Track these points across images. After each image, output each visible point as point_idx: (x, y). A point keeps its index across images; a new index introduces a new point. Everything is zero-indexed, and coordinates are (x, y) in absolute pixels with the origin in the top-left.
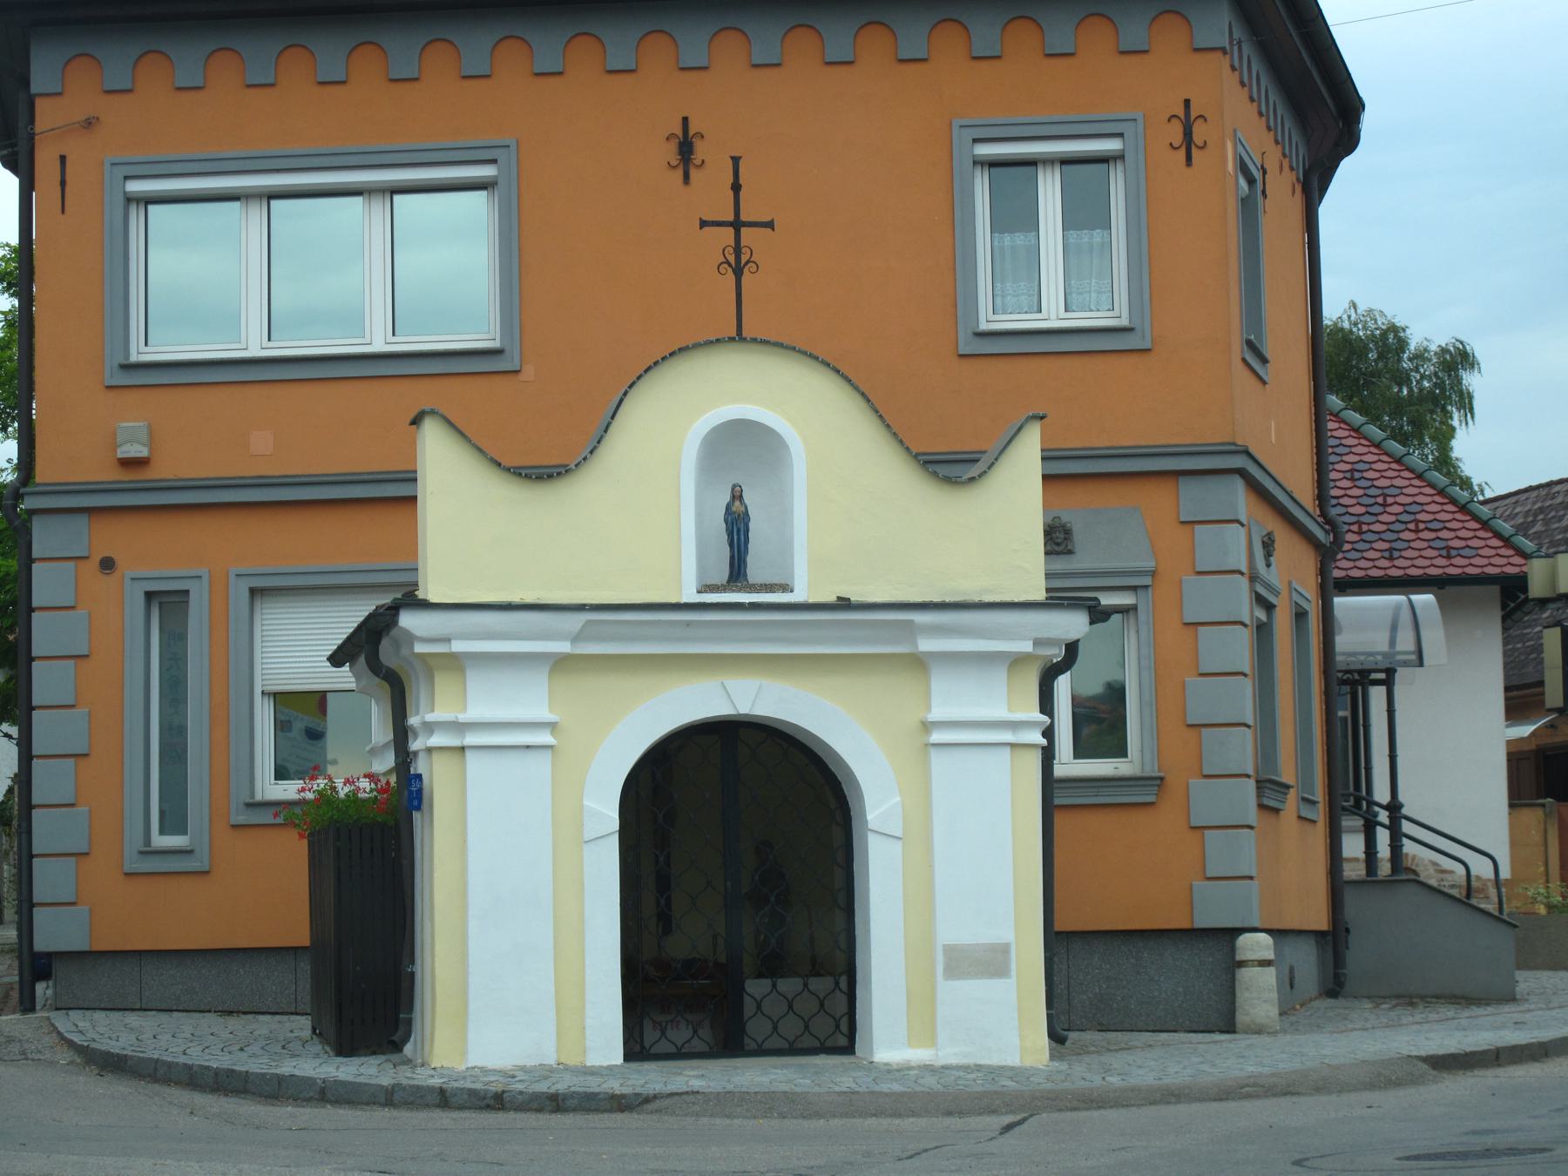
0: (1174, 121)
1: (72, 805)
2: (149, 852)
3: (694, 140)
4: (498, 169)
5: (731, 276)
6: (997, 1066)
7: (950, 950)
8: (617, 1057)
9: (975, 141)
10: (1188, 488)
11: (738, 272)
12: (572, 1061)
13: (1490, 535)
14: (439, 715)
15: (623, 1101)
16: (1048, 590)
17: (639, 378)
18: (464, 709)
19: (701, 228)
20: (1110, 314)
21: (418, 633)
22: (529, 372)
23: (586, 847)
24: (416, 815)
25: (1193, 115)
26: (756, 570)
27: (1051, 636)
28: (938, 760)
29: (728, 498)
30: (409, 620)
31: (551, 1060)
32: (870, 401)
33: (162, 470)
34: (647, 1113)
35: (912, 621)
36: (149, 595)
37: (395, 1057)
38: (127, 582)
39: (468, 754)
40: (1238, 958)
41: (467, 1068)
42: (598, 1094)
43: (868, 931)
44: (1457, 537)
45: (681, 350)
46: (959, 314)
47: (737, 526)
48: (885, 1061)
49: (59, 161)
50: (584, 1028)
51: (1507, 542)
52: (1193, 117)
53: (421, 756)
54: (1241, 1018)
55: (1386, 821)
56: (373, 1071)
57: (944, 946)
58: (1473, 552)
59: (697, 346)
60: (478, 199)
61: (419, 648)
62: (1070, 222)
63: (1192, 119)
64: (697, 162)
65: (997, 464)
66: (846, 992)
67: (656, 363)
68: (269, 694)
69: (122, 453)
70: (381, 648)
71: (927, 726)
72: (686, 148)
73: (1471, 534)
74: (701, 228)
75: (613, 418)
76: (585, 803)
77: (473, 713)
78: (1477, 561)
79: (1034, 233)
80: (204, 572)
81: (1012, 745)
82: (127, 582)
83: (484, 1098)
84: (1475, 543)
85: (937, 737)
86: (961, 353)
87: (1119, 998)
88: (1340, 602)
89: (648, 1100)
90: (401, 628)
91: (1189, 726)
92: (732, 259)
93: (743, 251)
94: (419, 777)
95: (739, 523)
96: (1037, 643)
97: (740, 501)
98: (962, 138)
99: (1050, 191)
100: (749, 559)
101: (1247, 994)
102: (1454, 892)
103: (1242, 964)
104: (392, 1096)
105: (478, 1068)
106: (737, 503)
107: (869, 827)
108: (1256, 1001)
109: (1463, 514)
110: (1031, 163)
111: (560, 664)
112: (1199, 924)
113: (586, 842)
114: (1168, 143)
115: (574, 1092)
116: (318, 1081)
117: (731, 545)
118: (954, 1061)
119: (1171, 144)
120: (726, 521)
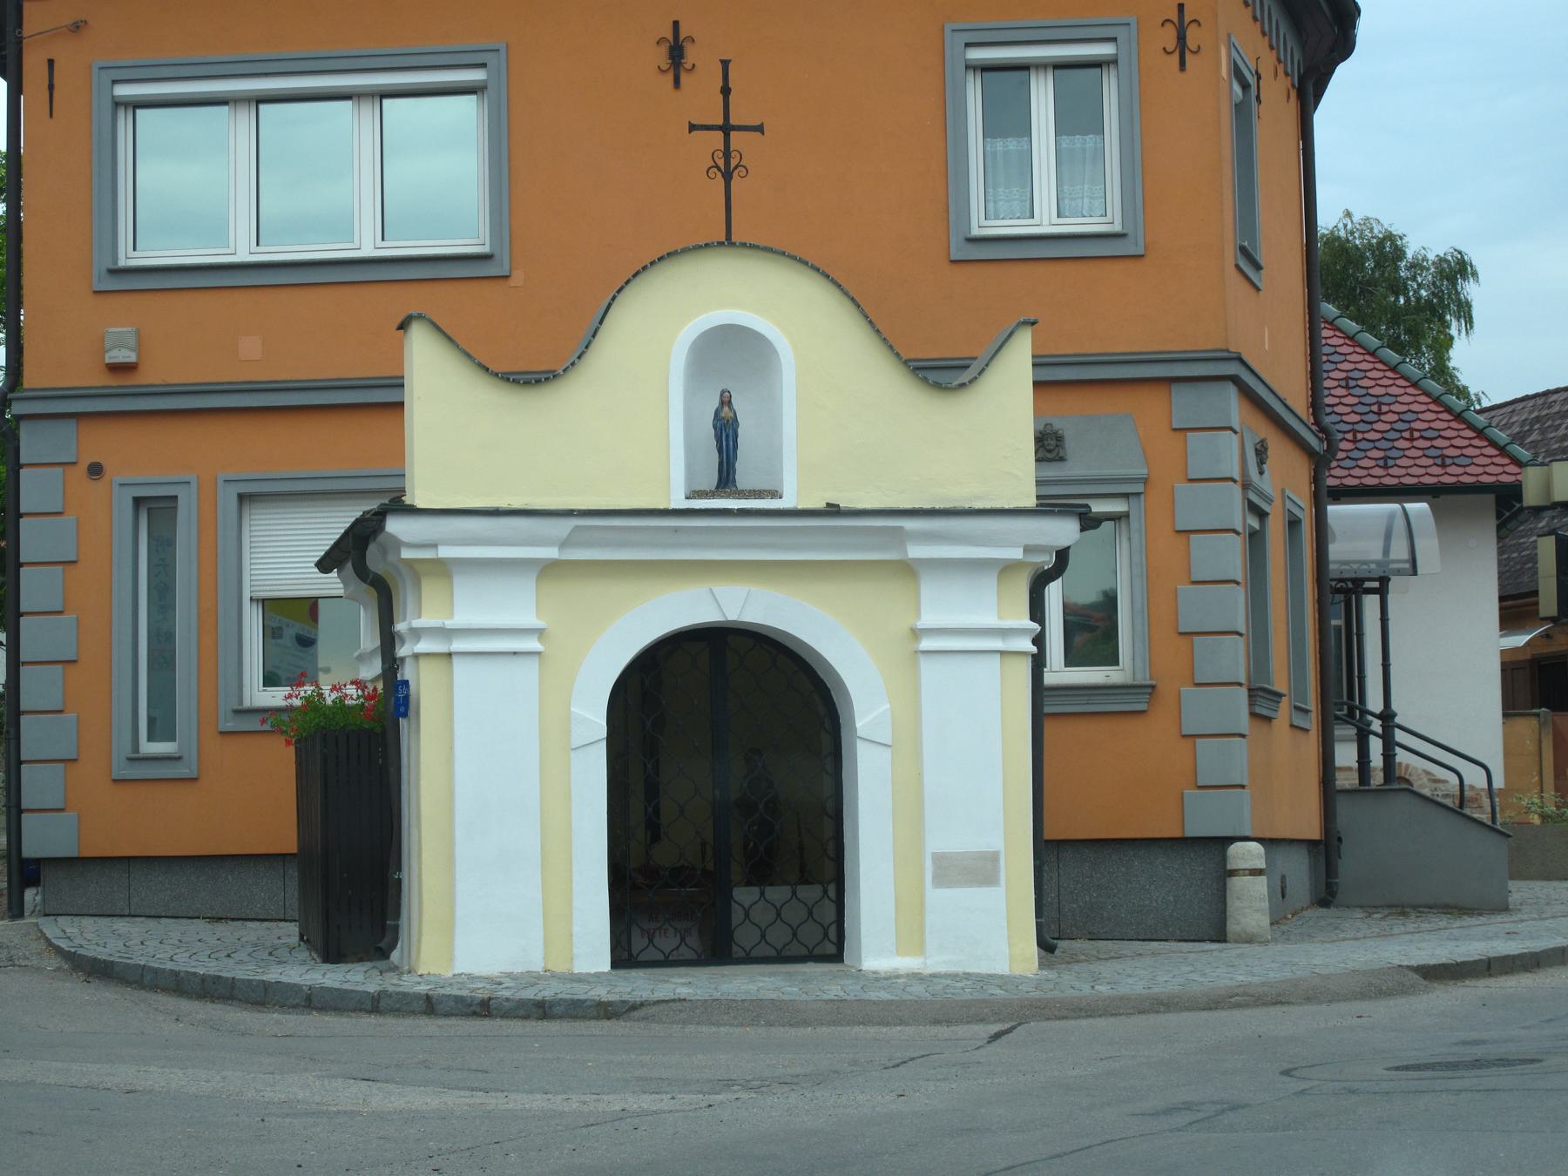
0: (1168, 25)
1: (61, 712)
2: (137, 759)
6: (987, 974)
7: (940, 860)
10: (1181, 395)
11: (728, 176)
12: (560, 967)
14: (425, 621)
16: (1038, 497)
17: (628, 282)
18: (452, 615)
19: (690, 132)
22: (518, 278)
23: (573, 754)
26: (743, 479)
28: (928, 668)
29: (716, 403)
30: (395, 526)
31: (537, 966)
33: (150, 376)
35: (901, 528)
36: (138, 502)
38: (116, 488)
39: (457, 663)
42: (585, 1001)
44: (1452, 446)
47: (726, 432)
50: (571, 935)
51: (1502, 450)
54: (1232, 928)
57: (933, 854)
59: (686, 251)
60: (466, 106)
61: (406, 554)
62: (1064, 125)
63: (1186, 24)
64: (688, 66)
67: (645, 268)
69: (110, 358)
70: (368, 553)
71: (917, 634)
74: (690, 132)
76: (572, 709)
77: (460, 619)
79: (1026, 139)
80: (192, 478)
81: (1002, 653)
82: (116, 488)
83: (471, 1005)
84: (1470, 452)
85: (927, 644)
86: (952, 259)
87: (1110, 907)
88: (1332, 509)
89: (635, 1007)
90: (388, 533)
91: (1181, 634)
92: (721, 163)
93: (733, 155)
94: (406, 683)
96: (1028, 549)
99: (1042, 96)
100: (737, 465)
101: (1238, 904)
103: (1233, 873)
106: (726, 409)
107: (859, 733)
110: (1023, 67)
111: (548, 570)
112: (1188, 834)
114: (1163, 46)
115: (560, 999)
117: (720, 450)
118: (942, 969)
119: (1164, 49)
120: (715, 427)
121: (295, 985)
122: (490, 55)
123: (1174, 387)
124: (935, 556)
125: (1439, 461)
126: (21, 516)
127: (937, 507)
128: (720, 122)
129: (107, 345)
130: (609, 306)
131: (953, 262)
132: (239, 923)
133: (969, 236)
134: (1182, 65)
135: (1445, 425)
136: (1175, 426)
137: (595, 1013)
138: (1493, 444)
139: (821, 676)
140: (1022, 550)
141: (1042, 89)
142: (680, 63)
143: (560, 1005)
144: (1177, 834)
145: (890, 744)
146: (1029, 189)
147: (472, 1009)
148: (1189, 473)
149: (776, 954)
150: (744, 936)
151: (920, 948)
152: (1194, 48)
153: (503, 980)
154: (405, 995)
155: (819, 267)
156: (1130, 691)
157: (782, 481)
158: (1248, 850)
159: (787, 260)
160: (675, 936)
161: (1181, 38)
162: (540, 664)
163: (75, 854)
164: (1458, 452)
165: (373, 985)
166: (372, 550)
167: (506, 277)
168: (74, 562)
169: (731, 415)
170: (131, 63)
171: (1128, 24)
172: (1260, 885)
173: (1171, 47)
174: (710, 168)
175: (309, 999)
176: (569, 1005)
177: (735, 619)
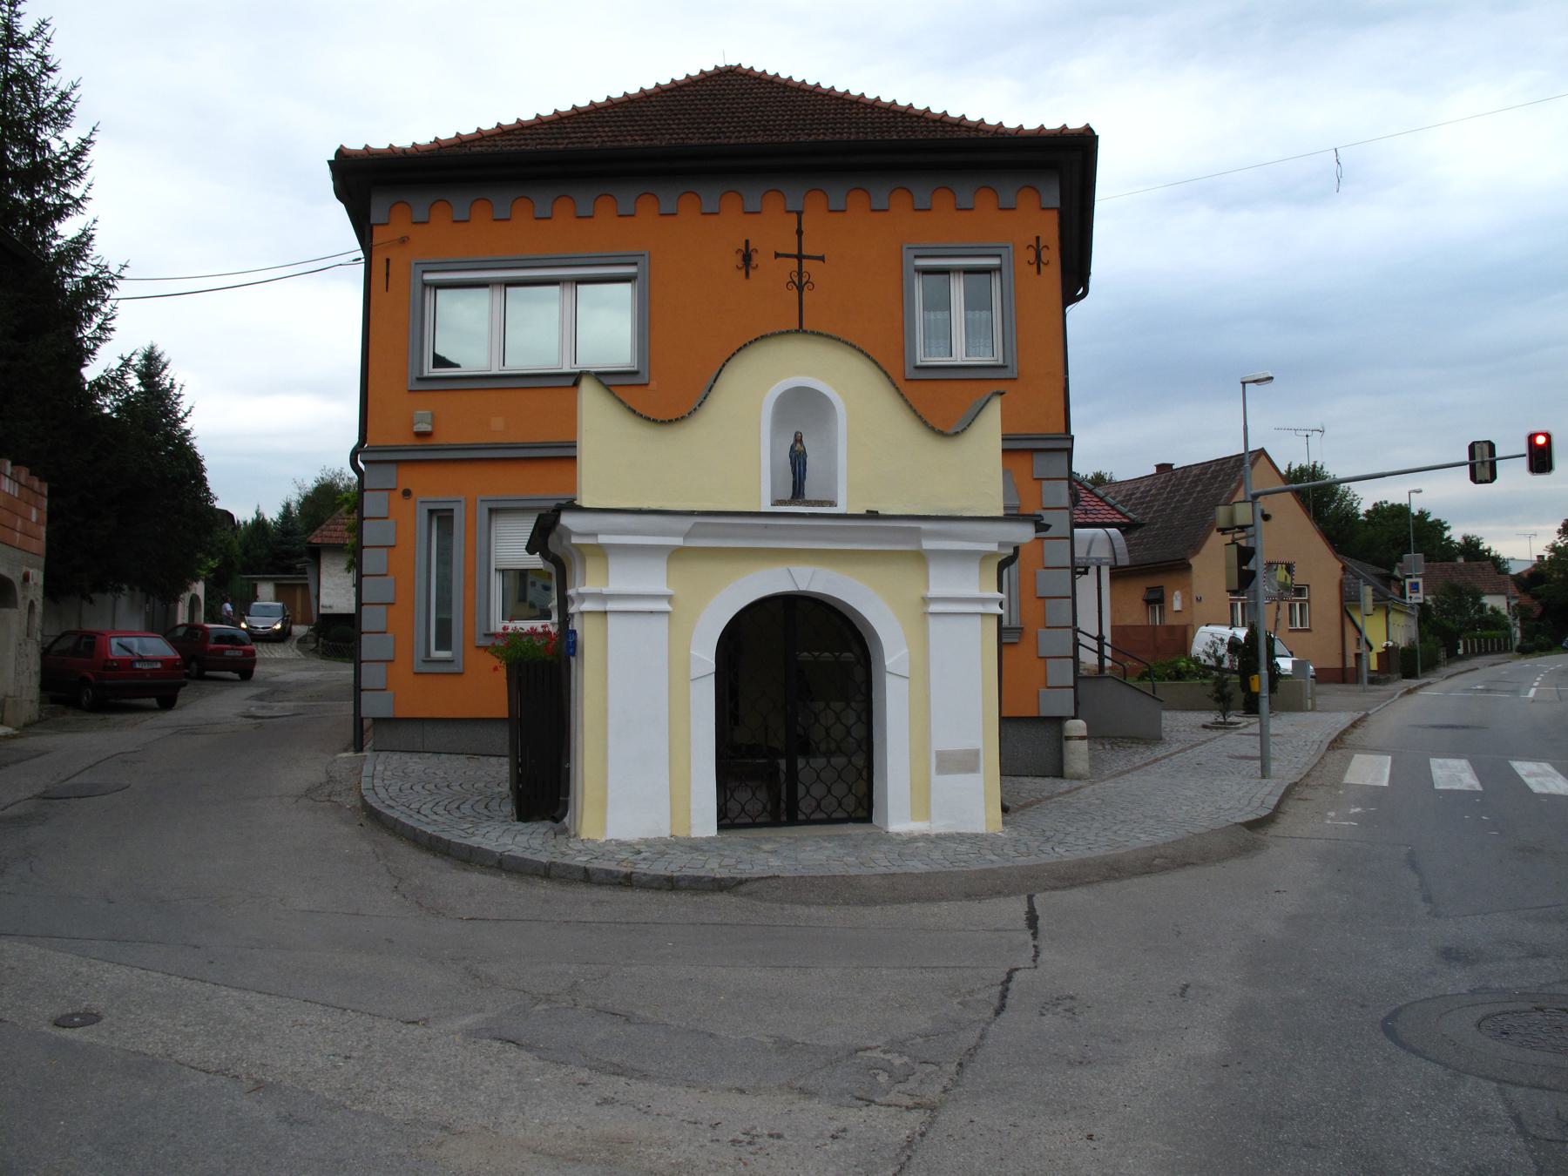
0: (1030, 248)
2: (428, 660)
5: (795, 291)
6: (972, 834)
7: (940, 754)
8: (710, 829)
9: (916, 257)
10: (1039, 460)
11: (800, 289)
12: (681, 833)
14: (589, 588)
16: (1005, 508)
17: (734, 355)
18: (607, 585)
19: (776, 258)
20: (993, 359)
21: (574, 529)
22: (653, 385)
24: (573, 659)
25: (1041, 245)
26: (810, 492)
28: (933, 623)
29: (791, 441)
30: (567, 520)
31: (666, 834)
33: (440, 439)
34: (741, 896)
35: (919, 528)
36: (431, 512)
37: (557, 826)
38: (418, 505)
39: (610, 618)
41: (606, 841)
42: (704, 877)
43: (884, 740)
45: (762, 337)
47: (798, 461)
50: (690, 811)
51: (1113, 508)
53: (576, 617)
54: (1068, 770)
55: (1106, 647)
56: (536, 843)
57: (937, 752)
58: (1097, 512)
59: (773, 335)
60: (625, 290)
61: (575, 540)
62: (969, 306)
64: (754, 265)
67: (745, 345)
68: (499, 570)
70: (550, 539)
71: (926, 601)
72: (747, 258)
74: (776, 258)
75: (715, 381)
76: (691, 652)
77: (614, 587)
78: (1099, 516)
80: (462, 498)
81: (982, 614)
82: (418, 505)
84: (1097, 508)
85: (933, 608)
88: (1077, 531)
89: (741, 882)
90: (562, 525)
92: (796, 280)
93: (804, 275)
94: (574, 632)
96: (1001, 545)
98: (908, 255)
99: (957, 287)
103: (1068, 738)
106: (798, 445)
107: (888, 669)
110: (945, 271)
111: (675, 554)
112: (1043, 714)
113: (692, 680)
117: (794, 474)
118: (942, 830)
119: (1029, 262)
121: (492, 852)
122: (639, 258)
127: (939, 514)
128: (796, 253)
130: (721, 370)
131: (907, 380)
132: (483, 759)
137: (711, 887)
138: (1108, 505)
144: (1036, 715)
145: (907, 676)
147: (619, 880)
148: (1044, 503)
150: (805, 805)
151: (927, 815)
153: (643, 848)
154: (568, 866)
157: (837, 494)
159: (842, 345)
161: (1038, 256)
162: (669, 619)
163: (392, 716)
164: (1092, 508)
165: (548, 854)
166: (552, 539)
167: (646, 385)
168: (394, 546)
169: (802, 449)
170: (427, 261)
175: (500, 862)
177: (805, 589)
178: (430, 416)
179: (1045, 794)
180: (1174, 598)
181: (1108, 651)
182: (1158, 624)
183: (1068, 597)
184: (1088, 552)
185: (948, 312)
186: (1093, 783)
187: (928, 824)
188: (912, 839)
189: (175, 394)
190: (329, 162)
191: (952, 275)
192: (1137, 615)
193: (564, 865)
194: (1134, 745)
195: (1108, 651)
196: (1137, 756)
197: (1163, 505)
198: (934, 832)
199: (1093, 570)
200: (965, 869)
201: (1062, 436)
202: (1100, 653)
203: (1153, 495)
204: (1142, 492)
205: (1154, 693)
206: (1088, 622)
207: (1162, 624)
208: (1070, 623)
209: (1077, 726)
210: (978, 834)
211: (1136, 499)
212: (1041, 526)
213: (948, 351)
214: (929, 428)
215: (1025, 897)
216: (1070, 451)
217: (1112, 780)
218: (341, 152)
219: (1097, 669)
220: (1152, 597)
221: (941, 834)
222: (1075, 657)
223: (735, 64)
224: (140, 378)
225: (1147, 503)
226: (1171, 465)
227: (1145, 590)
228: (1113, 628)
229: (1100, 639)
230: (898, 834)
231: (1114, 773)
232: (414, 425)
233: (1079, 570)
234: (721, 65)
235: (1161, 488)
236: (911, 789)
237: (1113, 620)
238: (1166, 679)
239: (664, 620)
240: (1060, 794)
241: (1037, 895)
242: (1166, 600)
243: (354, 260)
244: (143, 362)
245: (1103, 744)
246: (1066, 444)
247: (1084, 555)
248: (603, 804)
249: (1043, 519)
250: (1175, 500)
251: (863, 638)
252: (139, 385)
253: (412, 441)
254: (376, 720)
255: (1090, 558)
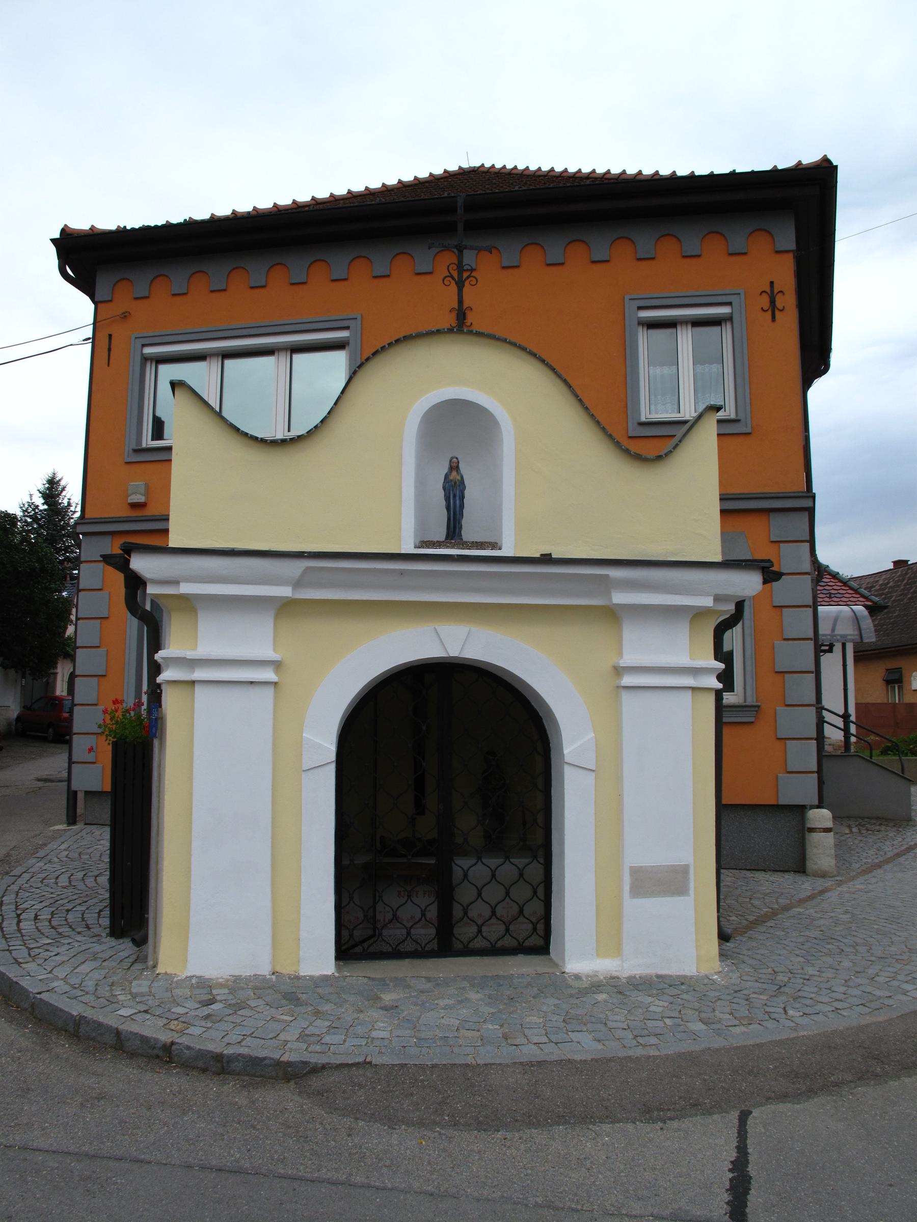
0: (764, 294)
1: (96, 705)
3: (466, 311)
4: (350, 332)
5: (454, 288)
7: (636, 872)
9: (640, 308)
10: (777, 521)
12: (287, 969)
13: (848, 588)
15: (289, 1069)
18: (195, 648)
23: (304, 775)
26: (469, 532)
27: (730, 593)
28: (629, 701)
29: (445, 470)
31: (265, 970)
32: (571, 387)
35: (607, 576)
40: (808, 825)
42: (265, 1059)
44: (833, 589)
46: (629, 414)
48: (576, 972)
49: (108, 338)
52: (776, 292)
54: (810, 865)
57: (631, 868)
58: (841, 596)
62: (697, 360)
63: (775, 294)
65: (681, 445)
66: (543, 936)
67: (383, 348)
69: (131, 499)
71: (619, 671)
73: (839, 588)
76: (304, 735)
77: (203, 650)
79: (675, 367)
81: (693, 689)
83: (154, 1048)
84: (841, 591)
85: (627, 680)
86: (630, 435)
87: (728, 848)
89: (316, 1070)
91: (777, 672)
92: (455, 275)
95: (455, 490)
96: (717, 599)
97: (457, 471)
98: (631, 306)
100: (464, 522)
101: (815, 850)
102: (839, 753)
103: (811, 830)
104: (79, 1029)
105: (197, 977)
106: (454, 473)
107: (567, 759)
108: (822, 856)
109: (835, 580)
112: (782, 802)
114: (760, 307)
115: (239, 1055)
116: (31, 995)
119: (762, 308)
120: (444, 488)
122: (351, 321)
123: (771, 514)
124: (637, 602)
125: (828, 595)
126: (79, 591)
129: (130, 492)
133: (639, 421)
134: (773, 319)
135: (829, 580)
136: (772, 539)
139: (535, 706)
140: (712, 598)
141: (684, 337)
142: (464, 323)
143: (238, 1061)
144: (773, 802)
145: (594, 769)
146: (677, 396)
147: (156, 1051)
149: (490, 946)
152: (781, 308)
155: (536, 352)
156: (745, 709)
158: (822, 816)
160: (424, 897)
161: (773, 302)
162: (275, 690)
164: (836, 592)
168: (107, 618)
169: (459, 478)
171: (739, 294)
172: (829, 838)
173: (766, 306)
174: (446, 277)
176: (247, 1062)
178: (143, 487)
179: (783, 901)
180: (912, 678)
181: (853, 729)
182: (897, 702)
183: (812, 672)
184: (833, 630)
185: (675, 367)
186: (840, 883)
187: (619, 963)
188: (596, 985)
189: (71, 511)
190: (53, 241)
191: (679, 328)
192: (877, 694)
193: (94, 1022)
194: (883, 828)
195: (853, 729)
196: (888, 843)
197: (901, 595)
198: (625, 974)
199: (838, 648)
200: (653, 1052)
201: (804, 494)
202: (846, 730)
203: (891, 587)
204: (881, 585)
205: (903, 773)
206: (833, 699)
207: (901, 702)
208: (813, 701)
209: (821, 817)
210: (685, 977)
211: (876, 591)
212: (770, 575)
213: (676, 407)
214: (623, 450)
215: (734, 1115)
216: (811, 511)
217: (861, 879)
218: (65, 231)
219: (843, 744)
220: (891, 677)
221: (634, 977)
222: (820, 738)
223: (478, 165)
224: (44, 498)
225: (886, 595)
226: (907, 561)
227: (885, 670)
228: (857, 705)
229: (846, 717)
230: (577, 977)
231: (864, 868)
232: (128, 496)
233: (823, 648)
234: (465, 165)
235: (899, 581)
236: (597, 915)
237: (856, 699)
238: (909, 754)
239: (269, 692)
240: (802, 902)
241: (755, 1113)
242: (905, 679)
243: (84, 340)
244: (47, 486)
245: (849, 827)
246: (807, 503)
247: (829, 632)
248: (184, 929)
249: (773, 566)
250: (911, 591)
251: (540, 719)
252: (43, 504)
253: (126, 513)
254: (88, 793)
255: (835, 636)
